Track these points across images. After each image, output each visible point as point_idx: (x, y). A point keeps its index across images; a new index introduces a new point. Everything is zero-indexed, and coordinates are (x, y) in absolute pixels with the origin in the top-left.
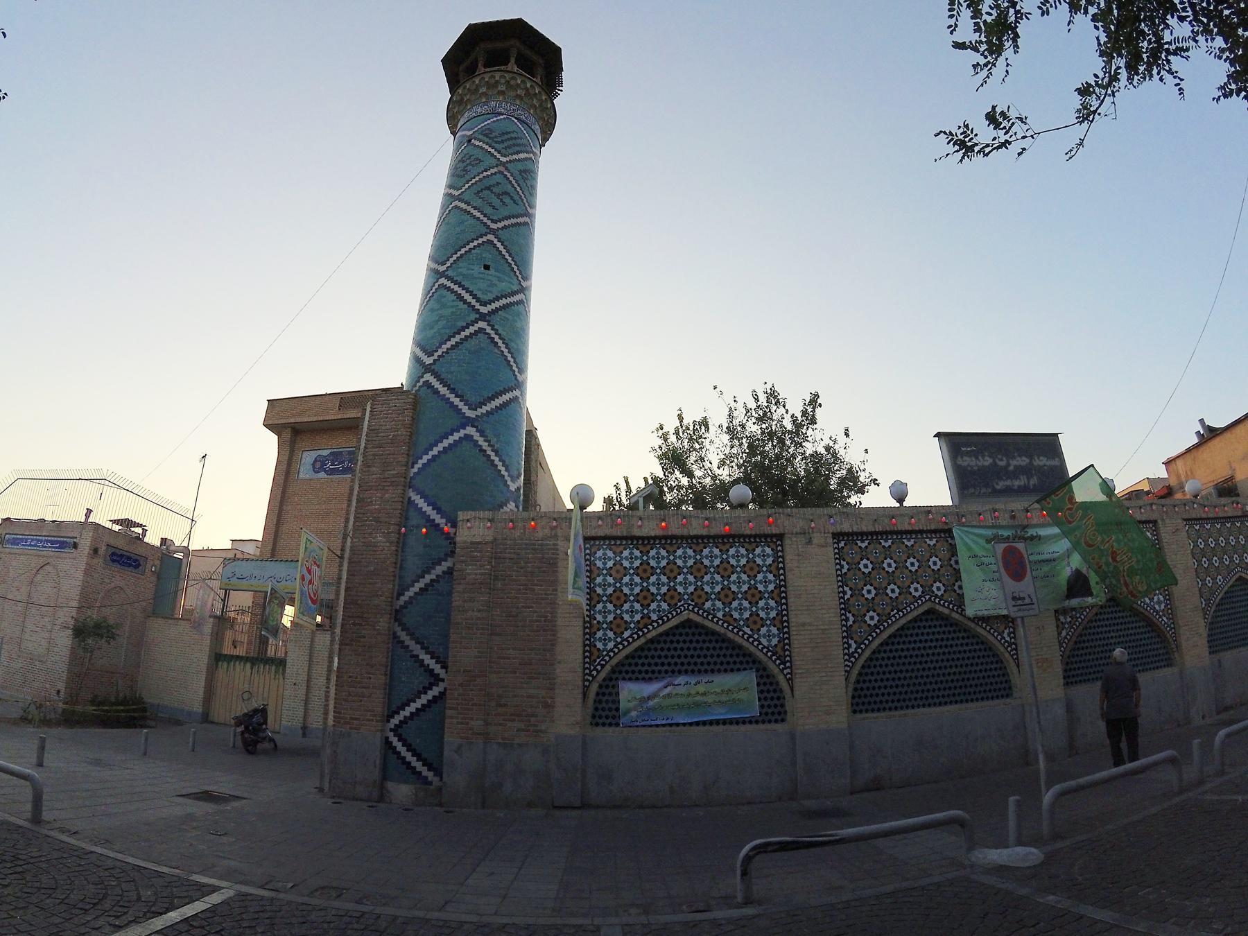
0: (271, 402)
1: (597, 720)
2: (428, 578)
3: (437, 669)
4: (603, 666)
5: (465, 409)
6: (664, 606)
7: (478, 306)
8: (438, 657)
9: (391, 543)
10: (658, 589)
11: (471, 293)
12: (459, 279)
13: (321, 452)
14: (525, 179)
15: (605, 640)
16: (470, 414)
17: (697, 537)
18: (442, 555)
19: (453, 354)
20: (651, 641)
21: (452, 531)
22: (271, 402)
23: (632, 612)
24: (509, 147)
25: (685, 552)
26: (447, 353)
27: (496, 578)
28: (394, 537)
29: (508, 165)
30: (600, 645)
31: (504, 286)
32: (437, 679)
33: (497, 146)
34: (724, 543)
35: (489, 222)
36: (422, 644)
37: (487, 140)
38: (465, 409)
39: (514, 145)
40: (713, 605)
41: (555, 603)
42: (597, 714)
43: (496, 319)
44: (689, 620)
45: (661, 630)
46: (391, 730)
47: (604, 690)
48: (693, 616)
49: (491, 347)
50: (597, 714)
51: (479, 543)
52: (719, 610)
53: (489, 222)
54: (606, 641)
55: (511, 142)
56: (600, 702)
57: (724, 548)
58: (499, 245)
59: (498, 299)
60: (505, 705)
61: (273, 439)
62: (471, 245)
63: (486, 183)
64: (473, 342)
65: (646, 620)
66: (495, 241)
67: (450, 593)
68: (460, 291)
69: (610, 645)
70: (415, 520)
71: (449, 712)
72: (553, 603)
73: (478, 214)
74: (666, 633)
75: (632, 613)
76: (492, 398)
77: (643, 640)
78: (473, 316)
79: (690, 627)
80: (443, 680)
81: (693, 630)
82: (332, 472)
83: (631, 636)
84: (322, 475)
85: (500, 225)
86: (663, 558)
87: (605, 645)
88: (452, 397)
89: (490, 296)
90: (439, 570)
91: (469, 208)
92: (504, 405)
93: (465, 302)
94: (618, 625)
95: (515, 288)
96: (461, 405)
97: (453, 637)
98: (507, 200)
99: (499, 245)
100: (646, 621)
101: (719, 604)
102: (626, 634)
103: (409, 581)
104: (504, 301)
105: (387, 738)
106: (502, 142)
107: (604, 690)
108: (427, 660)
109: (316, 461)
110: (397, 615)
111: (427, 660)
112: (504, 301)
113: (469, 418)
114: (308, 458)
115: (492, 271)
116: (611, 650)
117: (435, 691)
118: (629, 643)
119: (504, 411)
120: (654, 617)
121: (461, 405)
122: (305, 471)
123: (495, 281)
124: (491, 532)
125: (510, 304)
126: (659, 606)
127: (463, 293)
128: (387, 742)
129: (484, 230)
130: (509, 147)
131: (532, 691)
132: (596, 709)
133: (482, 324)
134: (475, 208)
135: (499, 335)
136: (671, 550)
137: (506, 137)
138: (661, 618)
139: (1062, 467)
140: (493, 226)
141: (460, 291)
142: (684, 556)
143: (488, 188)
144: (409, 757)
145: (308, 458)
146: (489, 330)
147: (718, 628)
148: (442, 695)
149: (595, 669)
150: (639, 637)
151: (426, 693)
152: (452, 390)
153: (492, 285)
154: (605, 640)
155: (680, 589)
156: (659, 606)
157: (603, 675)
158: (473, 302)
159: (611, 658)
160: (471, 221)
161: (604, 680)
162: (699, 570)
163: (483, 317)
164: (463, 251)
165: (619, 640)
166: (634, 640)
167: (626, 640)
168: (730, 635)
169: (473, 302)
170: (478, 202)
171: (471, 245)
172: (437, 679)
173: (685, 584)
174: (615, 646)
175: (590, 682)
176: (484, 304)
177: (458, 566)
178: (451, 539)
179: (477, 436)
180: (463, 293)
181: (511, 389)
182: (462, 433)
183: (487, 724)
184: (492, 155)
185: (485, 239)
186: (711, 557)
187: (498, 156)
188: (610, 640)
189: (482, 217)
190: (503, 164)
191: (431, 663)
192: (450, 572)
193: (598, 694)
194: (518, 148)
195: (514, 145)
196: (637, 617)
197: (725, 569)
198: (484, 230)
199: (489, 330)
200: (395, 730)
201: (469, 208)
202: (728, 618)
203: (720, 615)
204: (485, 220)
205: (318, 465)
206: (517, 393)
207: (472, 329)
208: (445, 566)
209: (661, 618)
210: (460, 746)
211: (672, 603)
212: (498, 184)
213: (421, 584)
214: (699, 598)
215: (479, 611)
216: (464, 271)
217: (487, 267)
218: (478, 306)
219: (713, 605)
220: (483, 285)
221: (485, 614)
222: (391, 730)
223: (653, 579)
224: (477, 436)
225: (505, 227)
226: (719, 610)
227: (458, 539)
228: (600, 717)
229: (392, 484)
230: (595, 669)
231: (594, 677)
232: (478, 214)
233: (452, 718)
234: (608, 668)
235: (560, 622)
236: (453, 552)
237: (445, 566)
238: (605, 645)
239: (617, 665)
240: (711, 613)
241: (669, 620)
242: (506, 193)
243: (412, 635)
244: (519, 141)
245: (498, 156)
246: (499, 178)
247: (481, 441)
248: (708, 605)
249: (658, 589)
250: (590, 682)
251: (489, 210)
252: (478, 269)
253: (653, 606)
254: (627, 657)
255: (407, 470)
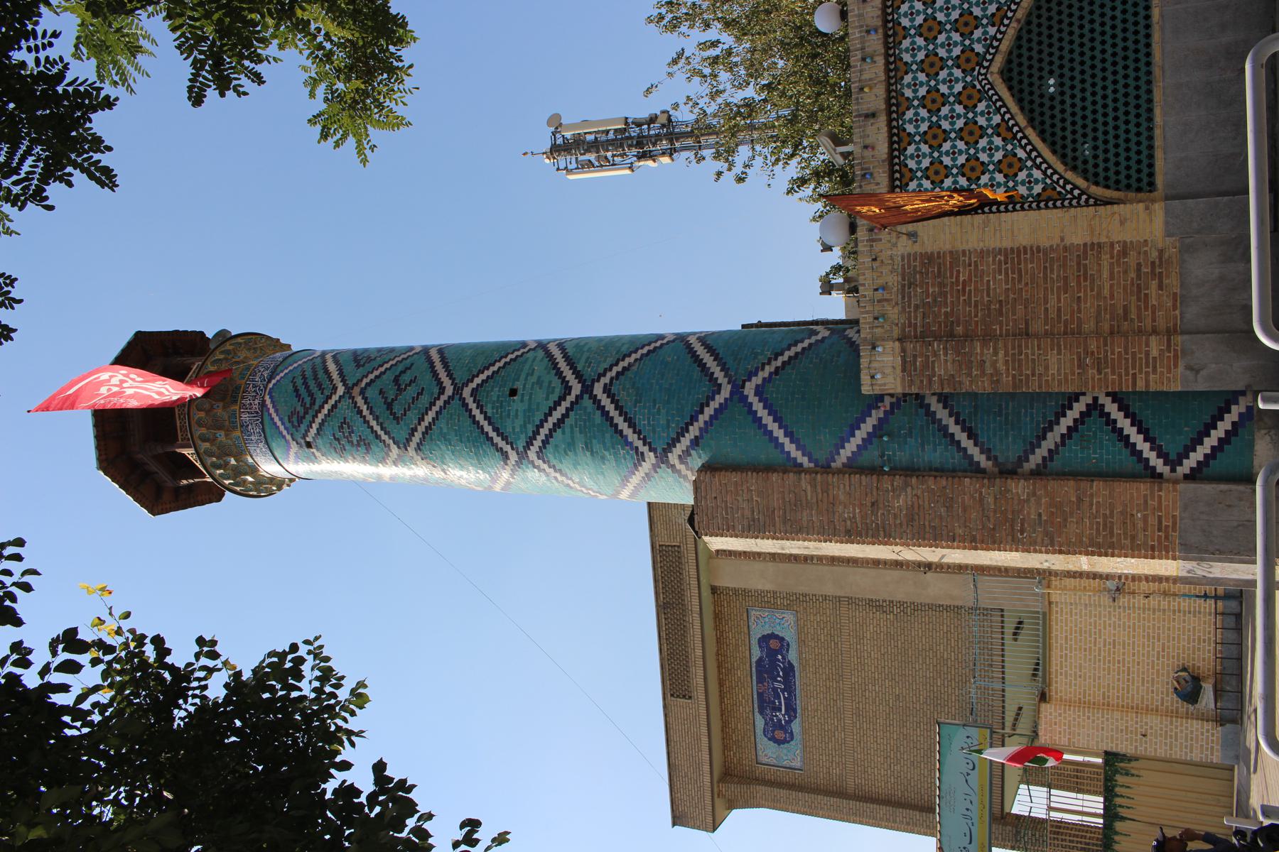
0: (677, 820)
1: (1144, 184)
2: (954, 429)
3: (1079, 407)
4: (1067, 182)
5: (719, 399)
6: (981, 107)
7: (571, 398)
8: (1063, 407)
9: (906, 485)
10: (959, 116)
11: (552, 410)
12: (530, 428)
13: (759, 730)
14: (369, 360)
15: (1030, 182)
16: (726, 392)
17: (887, 71)
18: (921, 411)
19: (642, 422)
20: (1031, 121)
21: (888, 400)
22: (677, 820)
23: (991, 149)
24: (320, 386)
25: (909, 86)
26: (639, 433)
27: (951, 335)
28: (898, 481)
29: (350, 383)
30: (1038, 189)
31: (540, 367)
32: (1095, 406)
33: (318, 403)
34: (895, 34)
35: (444, 397)
36: (1045, 432)
37: (308, 417)
38: (719, 399)
39: (316, 378)
40: (979, 41)
41: (982, 251)
42: (1135, 185)
43: (589, 373)
44: (1001, 73)
45: (1014, 108)
46: (1173, 470)
47: (1101, 179)
48: (996, 67)
49: (629, 374)
50: (1135, 185)
51: (903, 358)
52: (985, 33)
53: (444, 397)
54: (1031, 181)
55: (312, 384)
56: (1117, 182)
57: (901, 33)
58: (478, 381)
59: (559, 373)
60: (1126, 309)
61: (738, 819)
62: (480, 417)
63: (380, 408)
64: (622, 396)
65: (1002, 130)
66: (473, 385)
67: (974, 396)
68: (549, 425)
69: (1037, 174)
70: (872, 456)
71: (1141, 386)
72: (982, 254)
73: (431, 414)
74: (1020, 101)
75: (992, 149)
76: (702, 365)
77: (1030, 132)
78: (586, 402)
79: (1010, 70)
80: (1095, 399)
81: (1014, 65)
82: (791, 710)
83: (1024, 148)
84: (796, 727)
85: (447, 382)
86: (917, 114)
87: (1037, 181)
88: (703, 418)
89: (557, 383)
90: (942, 414)
91: (421, 429)
92: (711, 350)
93: (565, 416)
94: (1010, 166)
95: (541, 353)
96: (714, 405)
97: (1034, 387)
98: (406, 378)
99: (478, 381)
100: (1006, 131)
101: (978, 33)
102: (1021, 154)
103: (958, 456)
104: (562, 365)
105: (1186, 477)
106: (311, 395)
107: (1101, 179)
108: (1066, 422)
109: (773, 739)
110: (1009, 472)
111: (1066, 422)
112: (562, 365)
113: (732, 393)
114: (769, 752)
115: (519, 385)
116: (1044, 173)
117: (1112, 408)
118: (1034, 149)
119: (721, 352)
120: (997, 119)
121: (714, 405)
122: (789, 756)
123: (533, 379)
124: (889, 345)
125: (566, 357)
126: (982, 114)
127: (552, 420)
128: (1192, 476)
129: (456, 402)
130: (320, 386)
131: (1105, 274)
132: (1128, 187)
133: (598, 389)
134: (421, 420)
135: (606, 371)
136: (905, 104)
137: (302, 390)
138: (998, 110)
139: (1036, 784)
140: (449, 391)
141: (549, 425)
142: (914, 85)
143: (389, 406)
144: (1210, 442)
145: (769, 752)
146: (606, 380)
147: (1011, 33)
148: (1115, 397)
149: (1071, 192)
150: (1025, 137)
151: (1115, 421)
152: (693, 419)
153: (539, 382)
154: (1030, 182)
155: (958, 88)
156: (982, 114)
157: (1081, 182)
158: (565, 404)
159: (1055, 172)
160: (442, 423)
161: (1087, 179)
162: (932, 65)
163: (587, 389)
164: (488, 428)
165: (1029, 163)
166: (1030, 143)
167: (1029, 154)
168: (1019, 14)
169: (565, 404)
170: (412, 416)
171: (480, 417)
172: (1095, 406)
173: (950, 81)
174: (1038, 168)
175: (1089, 197)
176: (568, 389)
177: (936, 388)
178: (900, 401)
179: (757, 380)
180: (552, 420)
181: (689, 346)
182: (753, 399)
183: (1155, 332)
184: (334, 407)
185: (470, 401)
186: (913, 50)
187: (335, 398)
188: (1030, 175)
189: (436, 408)
190: (349, 390)
191: (1072, 415)
192: (944, 399)
193: (1107, 187)
194: (321, 374)
195: (316, 378)
196: (998, 141)
197: (930, 29)
198: (456, 402)
199: (606, 380)
200: (1174, 463)
201: (421, 429)
202: (997, 20)
203: (992, 31)
204: (440, 403)
205: (779, 734)
206: (692, 340)
207: (606, 402)
208: (936, 406)
209: (998, 110)
210: (1189, 368)
211: (977, 96)
212: (381, 392)
213: (962, 437)
214: (969, 61)
215: (996, 353)
216: (519, 422)
217: (513, 392)
218: (571, 398)
219: (979, 41)
220: (540, 395)
221: (1000, 344)
222: (1173, 470)
223: (945, 125)
224: (757, 380)
225: (450, 375)
226: (985, 33)
227: (899, 390)
228: (1139, 180)
229: (825, 491)
230: (1071, 192)
231: (1083, 193)
232: (431, 414)
233: (1147, 382)
234: (1069, 175)
235: (1007, 244)
236: (919, 397)
237: (936, 406)
238: (1037, 181)
239: (1065, 164)
240: (990, 43)
241: (1000, 99)
242: (396, 380)
243: (1033, 447)
244: (309, 373)
245: (335, 398)
246: (372, 393)
247: (765, 374)
248: (979, 48)
249: (959, 116)
250: (1089, 197)
251: (425, 400)
252: (517, 404)
253: (982, 121)
254: (1054, 152)
255: (807, 471)
